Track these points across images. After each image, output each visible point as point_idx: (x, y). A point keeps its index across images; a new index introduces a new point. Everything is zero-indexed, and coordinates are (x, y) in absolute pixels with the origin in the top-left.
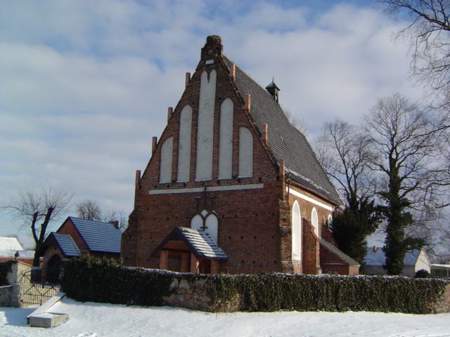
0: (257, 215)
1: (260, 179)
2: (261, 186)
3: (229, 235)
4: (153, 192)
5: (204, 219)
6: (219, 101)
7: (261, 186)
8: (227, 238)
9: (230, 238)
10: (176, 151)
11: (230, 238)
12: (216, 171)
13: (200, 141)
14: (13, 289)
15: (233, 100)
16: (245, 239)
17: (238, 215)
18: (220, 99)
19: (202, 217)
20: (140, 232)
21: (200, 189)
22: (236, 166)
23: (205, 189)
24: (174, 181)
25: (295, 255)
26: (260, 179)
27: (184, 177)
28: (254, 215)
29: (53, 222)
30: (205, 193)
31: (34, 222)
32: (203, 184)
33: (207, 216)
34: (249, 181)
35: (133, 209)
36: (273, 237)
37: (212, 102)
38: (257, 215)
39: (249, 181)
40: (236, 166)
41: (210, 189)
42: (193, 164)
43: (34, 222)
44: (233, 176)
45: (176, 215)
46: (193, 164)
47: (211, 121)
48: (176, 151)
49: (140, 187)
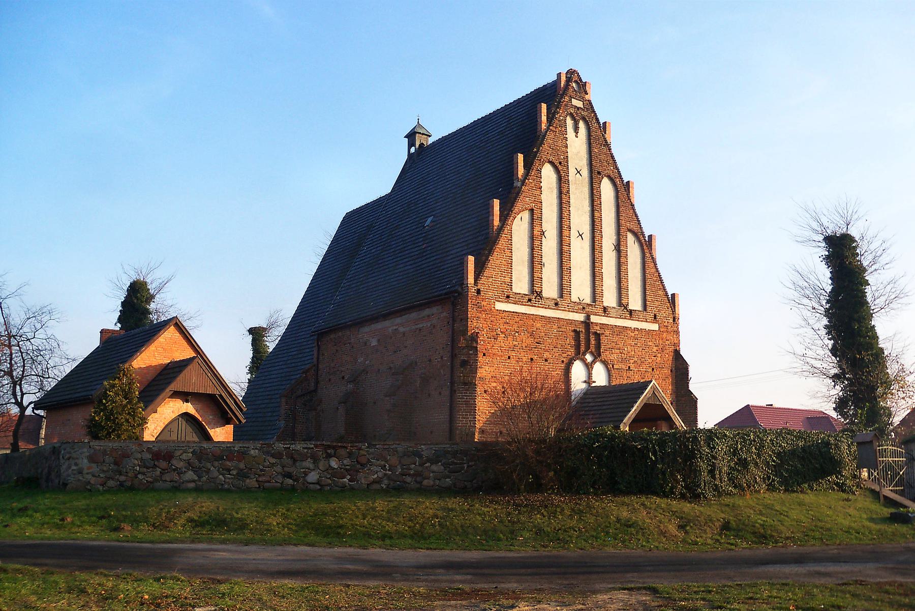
0: (653, 369)
2: (655, 327)
4: (500, 306)
5: (589, 367)
7: (655, 327)
17: (632, 366)
21: (580, 317)
23: (588, 317)
27: (550, 289)
33: (594, 362)
38: (653, 369)
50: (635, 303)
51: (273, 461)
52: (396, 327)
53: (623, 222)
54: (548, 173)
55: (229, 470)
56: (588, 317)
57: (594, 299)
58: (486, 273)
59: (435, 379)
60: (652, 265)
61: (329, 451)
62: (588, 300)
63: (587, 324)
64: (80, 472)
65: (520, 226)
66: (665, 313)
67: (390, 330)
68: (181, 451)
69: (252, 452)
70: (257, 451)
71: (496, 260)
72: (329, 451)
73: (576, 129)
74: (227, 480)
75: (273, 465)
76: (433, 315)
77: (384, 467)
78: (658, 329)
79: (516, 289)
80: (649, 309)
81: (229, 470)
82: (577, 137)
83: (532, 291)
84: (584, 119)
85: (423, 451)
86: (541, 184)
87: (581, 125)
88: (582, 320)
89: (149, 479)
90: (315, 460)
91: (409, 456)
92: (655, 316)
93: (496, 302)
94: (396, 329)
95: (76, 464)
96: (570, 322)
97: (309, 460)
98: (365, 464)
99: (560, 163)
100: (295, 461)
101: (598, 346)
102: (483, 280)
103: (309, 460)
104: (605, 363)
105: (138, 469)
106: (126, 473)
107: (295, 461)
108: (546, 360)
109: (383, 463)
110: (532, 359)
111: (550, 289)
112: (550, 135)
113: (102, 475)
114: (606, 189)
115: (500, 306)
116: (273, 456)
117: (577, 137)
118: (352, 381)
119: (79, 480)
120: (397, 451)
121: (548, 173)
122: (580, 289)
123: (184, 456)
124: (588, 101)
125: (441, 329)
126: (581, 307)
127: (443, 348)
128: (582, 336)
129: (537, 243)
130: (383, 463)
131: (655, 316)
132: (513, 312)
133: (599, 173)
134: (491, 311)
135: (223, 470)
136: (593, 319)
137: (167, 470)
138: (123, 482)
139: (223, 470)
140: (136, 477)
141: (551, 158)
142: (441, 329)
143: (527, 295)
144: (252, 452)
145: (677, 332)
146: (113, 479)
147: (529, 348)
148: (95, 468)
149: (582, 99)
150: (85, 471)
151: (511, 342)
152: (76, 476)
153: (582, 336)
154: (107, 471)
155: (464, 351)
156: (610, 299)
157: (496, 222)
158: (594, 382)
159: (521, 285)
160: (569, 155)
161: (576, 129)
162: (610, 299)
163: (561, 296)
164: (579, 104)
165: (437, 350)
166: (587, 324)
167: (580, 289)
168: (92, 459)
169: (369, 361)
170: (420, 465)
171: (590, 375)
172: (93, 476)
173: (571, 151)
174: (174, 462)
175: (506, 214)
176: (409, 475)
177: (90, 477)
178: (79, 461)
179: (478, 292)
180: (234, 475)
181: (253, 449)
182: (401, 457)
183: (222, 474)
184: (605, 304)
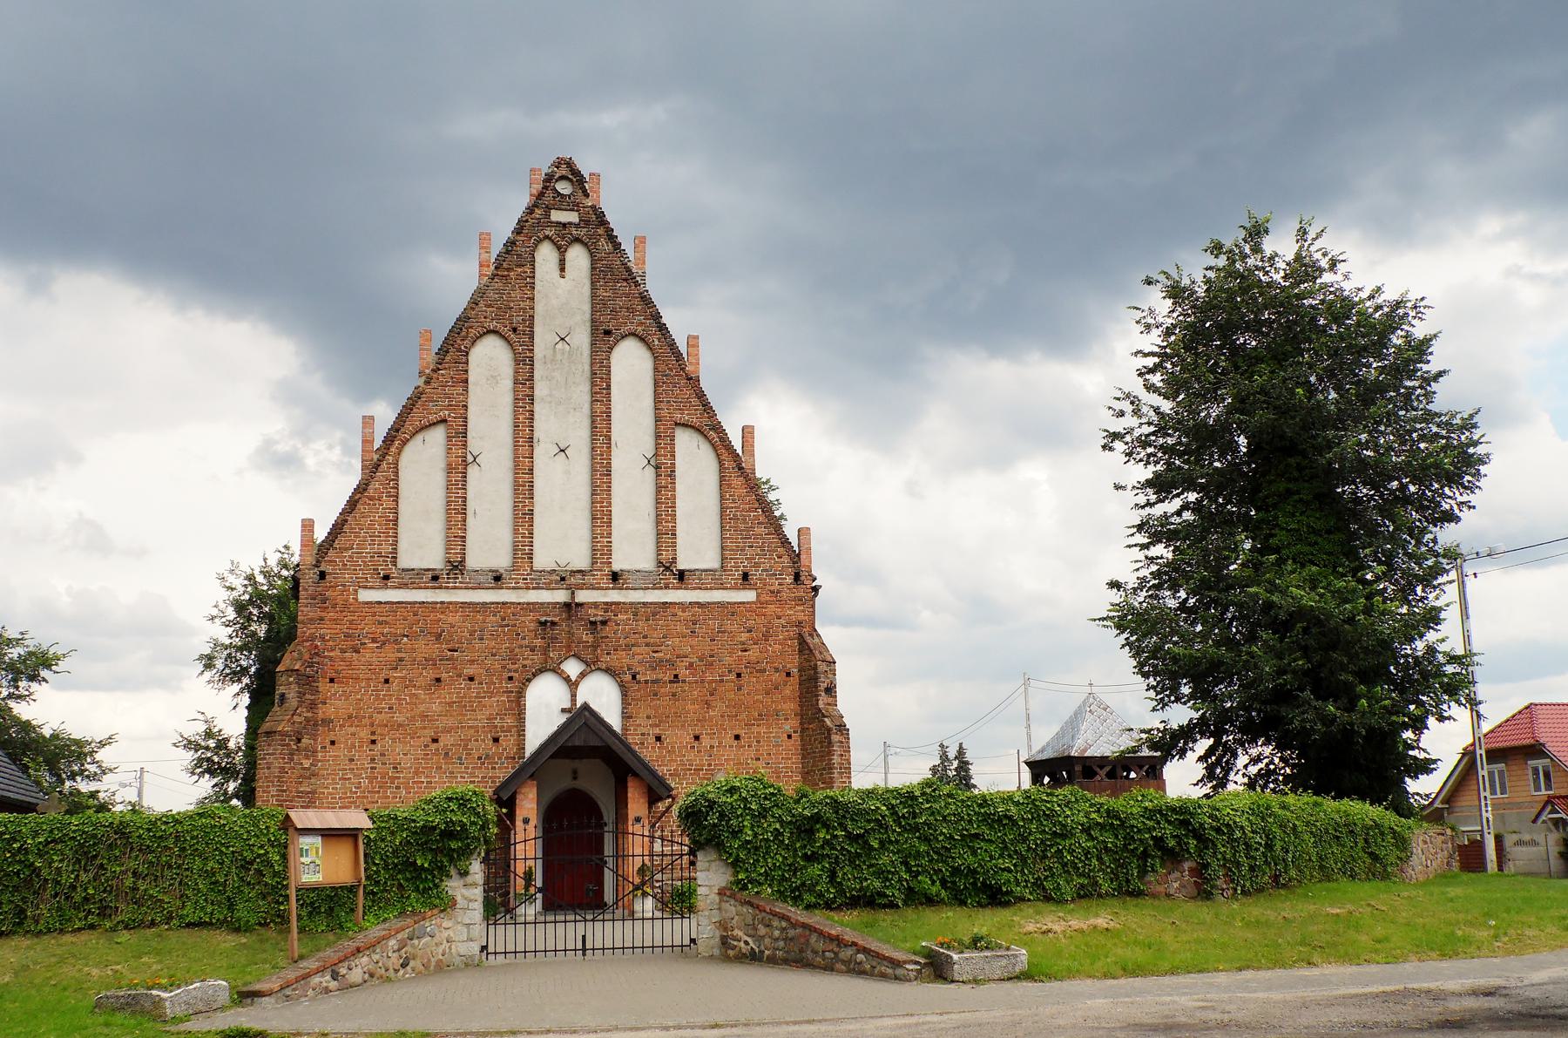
0: (739, 675)
1: (745, 576)
2: (749, 596)
3: (657, 731)
4: (365, 596)
6: (604, 337)
8: (652, 740)
9: (658, 739)
10: (458, 469)
11: (658, 739)
12: (601, 547)
13: (543, 453)
14: (1458, 517)
15: (650, 347)
16: (706, 741)
17: (683, 673)
18: (608, 333)
19: (567, 679)
20: (327, 722)
21: (561, 596)
22: (665, 532)
24: (456, 567)
25: (1491, 855)
26: (745, 576)
28: (733, 677)
29: (61, 687)
30: (569, 607)
31: (1521, 874)
32: (562, 578)
34: (713, 579)
35: (598, 760)
36: (789, 737)
37: (582, 338)
38: (739, 675)
39: (713, 579)
40: (665, 532)
41: (583, 596)
42: (523, 516)
43: (1521, 874)
44: (660, 563)
45: (469, 671)
46: (523, 516)
47: (579, 436)
48: (458, 469)
49: (565, 728)
79: (754, 599)
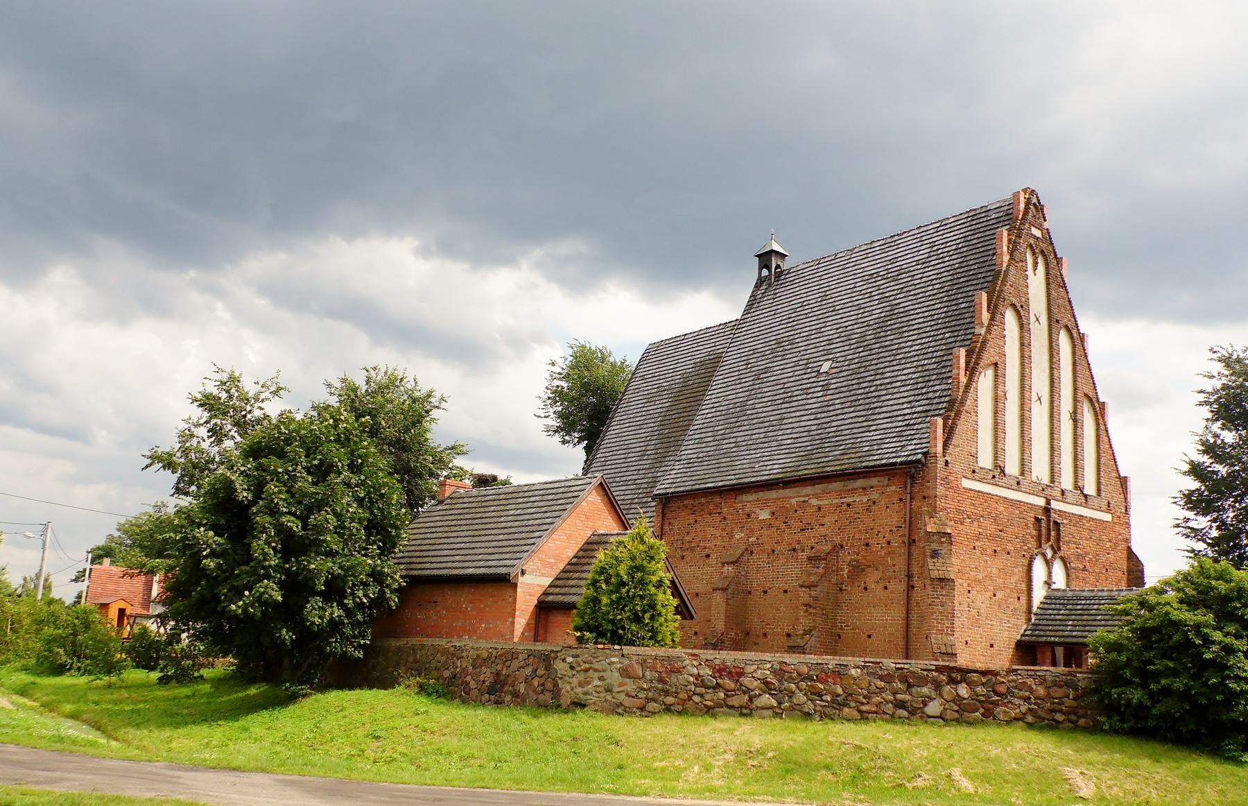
4: (967, 484)
23: (1048, 502)
27: (1012, 468)
50: (1090, 489)
51: (881, 684)
52: (807, 499)
53: (1079, 385)
54: (1010, 317)
55: (820, 695)
56: (1048, 502)
57: (1052, 481)
58: (954, 441)
59: (877, 569)
60: (1106, 439)
61: (954, 675)
62: (1046, 480)
63: (1047, 510)
64: (609, 690)
65: (985, 381)
66: (1117, 499)
67: (794, 501)
68: (755, 667)
69: (853, 672)
70: (859, 670)
71: (962, 426)
72: (954, 675)
73: (1035, 265)
74: (818, 708)
75: (881, 689)
76: (872, 487)
77: (1027, 699)
78: (1111, 520)
80: (1103, 494)
81: (820, 695)
82: (1035, 275)
83: (996, 466)
84: (1042, 252)
85: (1079, 681)
86: (1005, 333)
87: (1040, 260)
88: (582, 455)
89: (709, 703)
90: (938, 686)
91: (1060, 687)
92: (1109, 503)
93: (963, 479)
94: (804, 502)
95: (600, 678)
96: (1032, 507)
97: (929, 685)
98: (1004, 694)
99: (1022, 307)
100: (910, 686)
101: (1058, 539)
102: (951, 449)
103: (929, 685)
104: (1062, 559)
105: (693, 689)
106: (676, 693)
107: (910, 686)
108: (1008, 553)
109: (1027, 694)
110: (995, 551)
111: (1012, 468)
112: (1013, 271)
113: (640, 695)
114: (1063, 340)
115: (967, 484)
116: (881, 678)
117: (1035, 275)
118: (731, 563)
119: (606, 700)
120: (1045, 680)
121: (1010, 317)
122: (1040, 470)
123: (759, 674)
124: (1047, 229)
125: (887, 507)
126: (1042, 490)
127: (891, 531)
128: (1044, 524)
129: (1000, 405)
130: (1027, 694)
131: (1109, 503)
132: (979, 492)
133: (1057, 321)
134: (958, 490)
135: (811, 694)
136: (1054, 505)
137: (734, 691)
138: (671, 705)
139: (811, 694)
140: (690, 698)
141: (1014, 301)
142: (887, 507)
143: (990, 470)
144: (853, 672)
145: (1128, 525)
146: (656, 701)
147: (992, 538)
148: (630, 686)
149: (1040, 228)
150: (616, 689)
151: (975, 529)
152: (602, 695)
153: (1044, 524)
154: (648, 690)
155: (935, 538)
156: (1066, 482)
157: (963, 380)
158: (1054, 583)
159: (985, 460)
160: (1031, 296)
161: (1035, 265)
162: (1066, 482)
163: (1022, 474)
164: (1036, 232)
165: (879, 532)
166: (1047, 510)
167: (1040, 470)
168: (625, 673)
169: (755, 539)
170: (1074, 699)
171: (1050, 574)
172: (627, 695)
173: (1031, 291)
174: (746, 681)
175: (972, 370)
176: (1060, 711)
177: (622, 697)
178: (606, 675)
179: (947, 463)
180: (828, 702)
181: (854, 668)
182: (1050, 687)
183: (811, 700)
184: (1063, 487)
